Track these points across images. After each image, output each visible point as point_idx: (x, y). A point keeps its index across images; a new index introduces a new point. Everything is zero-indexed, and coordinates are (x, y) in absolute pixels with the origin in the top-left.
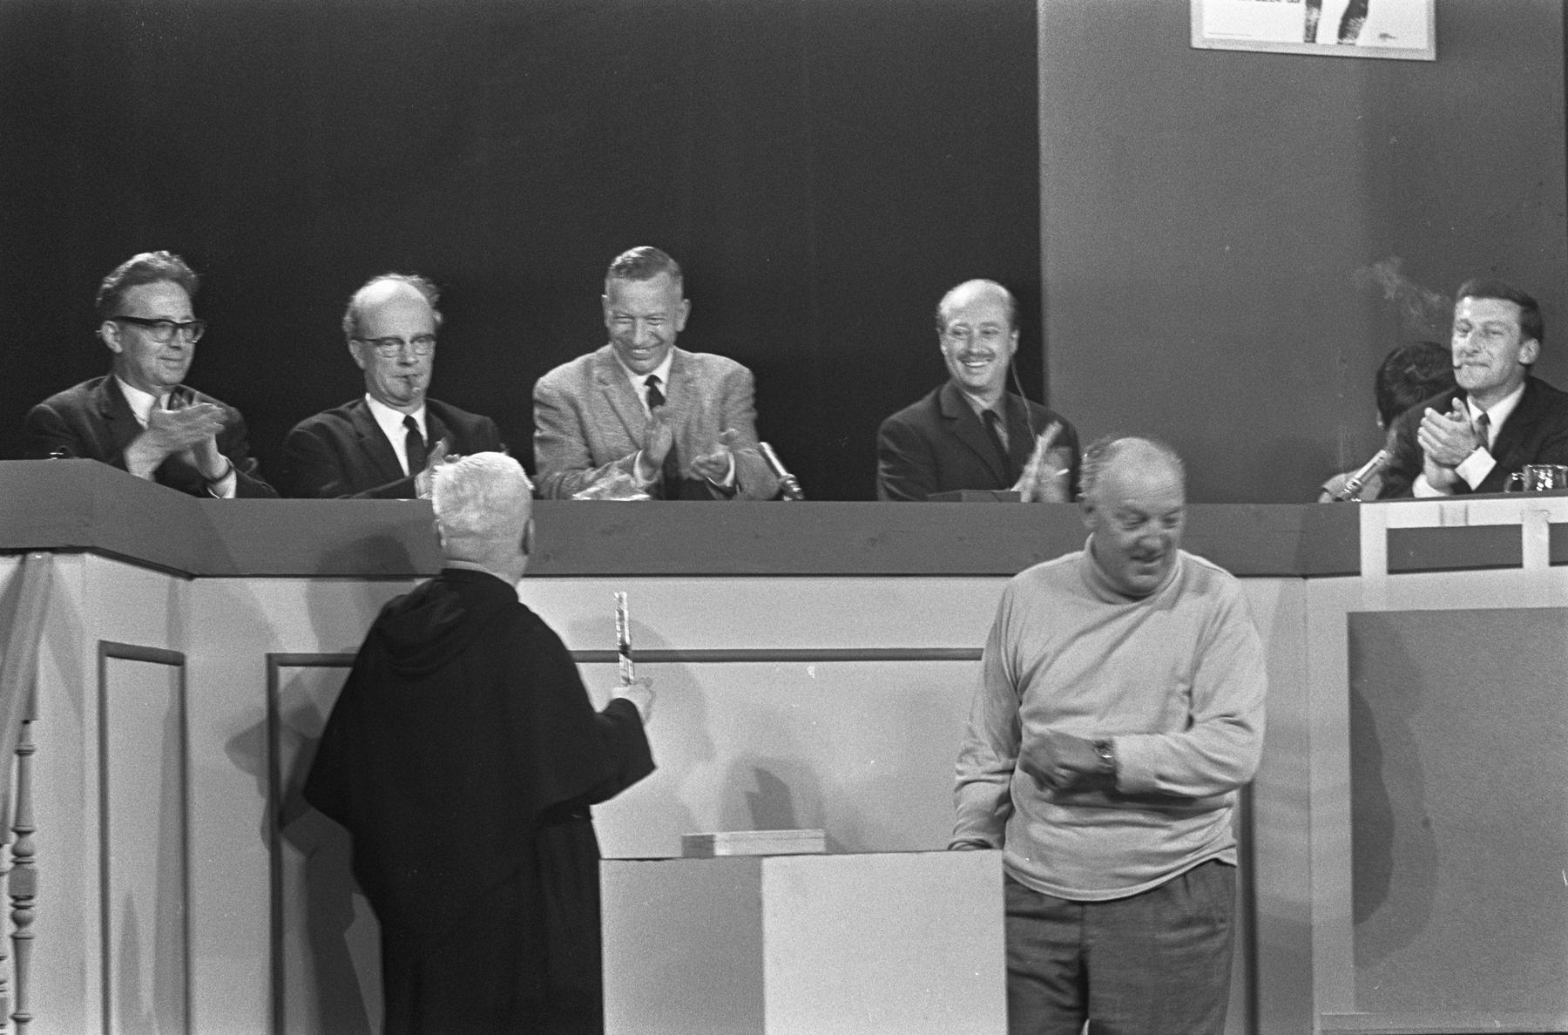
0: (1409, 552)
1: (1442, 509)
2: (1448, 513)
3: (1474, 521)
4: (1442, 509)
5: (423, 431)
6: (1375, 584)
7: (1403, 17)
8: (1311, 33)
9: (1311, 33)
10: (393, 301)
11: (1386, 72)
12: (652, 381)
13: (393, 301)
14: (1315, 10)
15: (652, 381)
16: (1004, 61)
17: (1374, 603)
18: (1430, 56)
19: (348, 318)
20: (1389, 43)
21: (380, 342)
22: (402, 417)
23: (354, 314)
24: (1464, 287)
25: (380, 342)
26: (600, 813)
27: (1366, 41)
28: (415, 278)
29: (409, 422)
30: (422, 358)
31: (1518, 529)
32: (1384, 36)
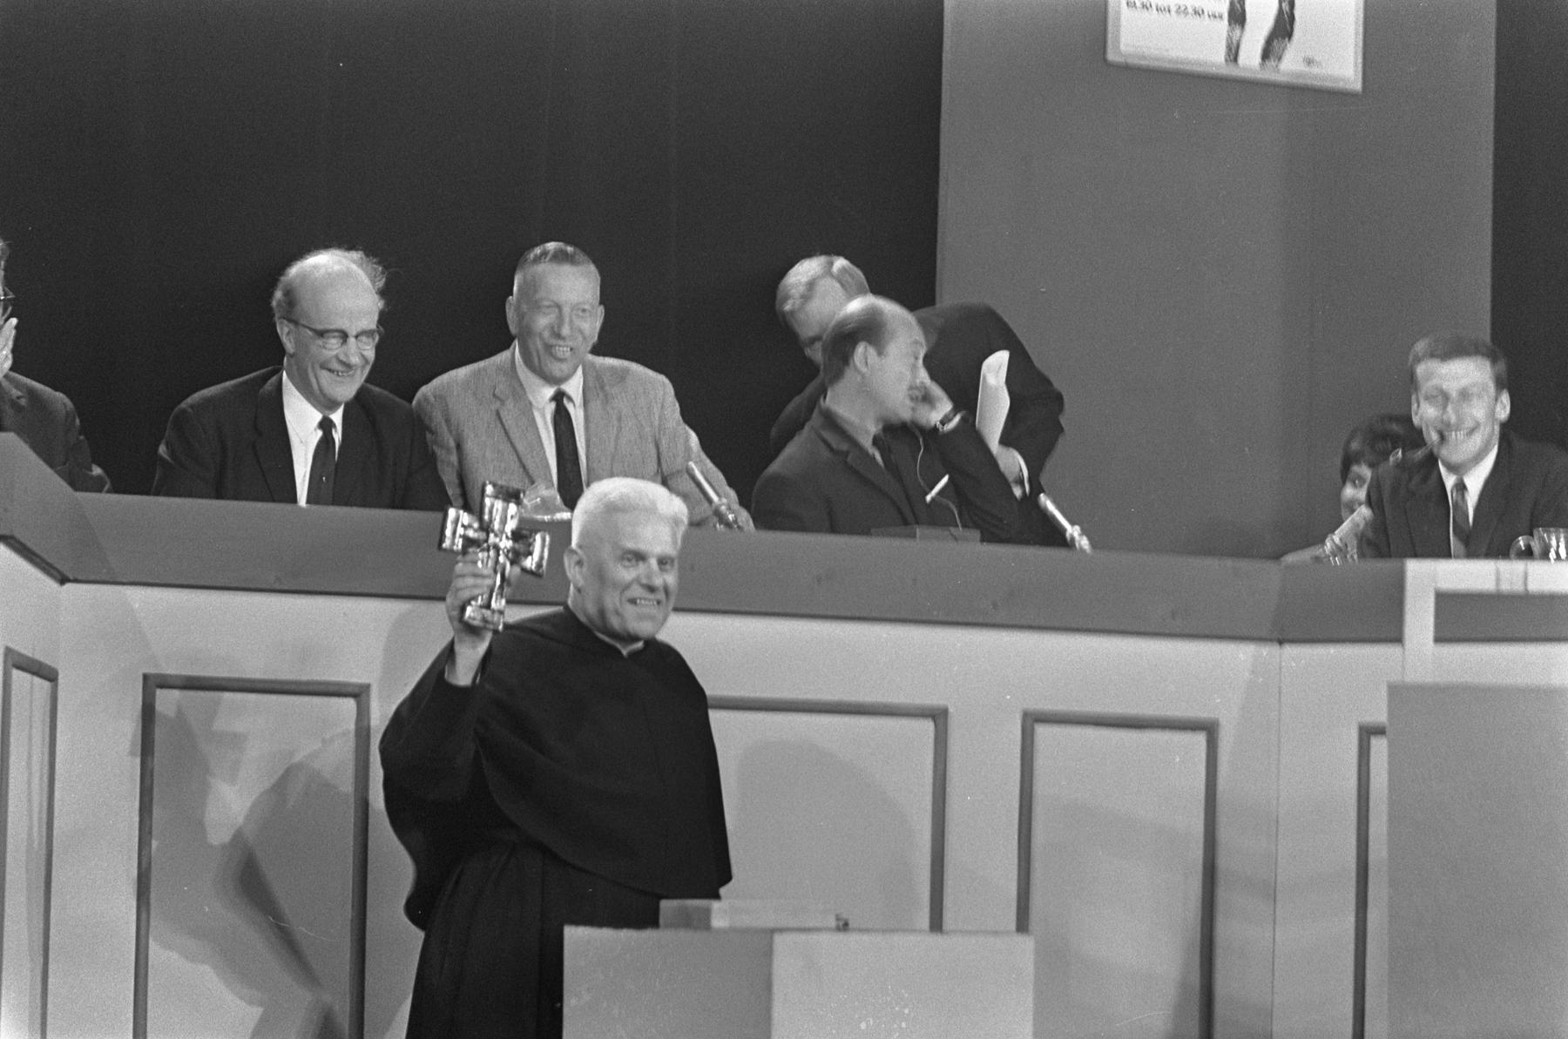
0: (1462, 618)
1: (1498, 573)
2: (1505, 576)
3: (1534, 587)
4: (1498, 573)
5: (337, 436)
6: (1421, 652)
7: (1332, 46)
8: (1233, 53)
9: (1233, 53)
10: (339, 284)
11: (1310, 98)
12: (559, 397)
13: (339, 284)
14: (1238, 32)
15: (559, 397)
16: (918, 52)
17: (1415, 675)
18: (1357, 86)
19: (278, 294)
20: (1315, 70)
21: (321, 334)
22: (318, 416)
23: (288, 293)
24: (1420, 346)
25: (321, 334)
26: (421, 935)
27: (1291, 64)
28: (356, 255)
29: (326, 425)
30: (363, 352)
31: (1398, 639)
32: (1309, 62)
